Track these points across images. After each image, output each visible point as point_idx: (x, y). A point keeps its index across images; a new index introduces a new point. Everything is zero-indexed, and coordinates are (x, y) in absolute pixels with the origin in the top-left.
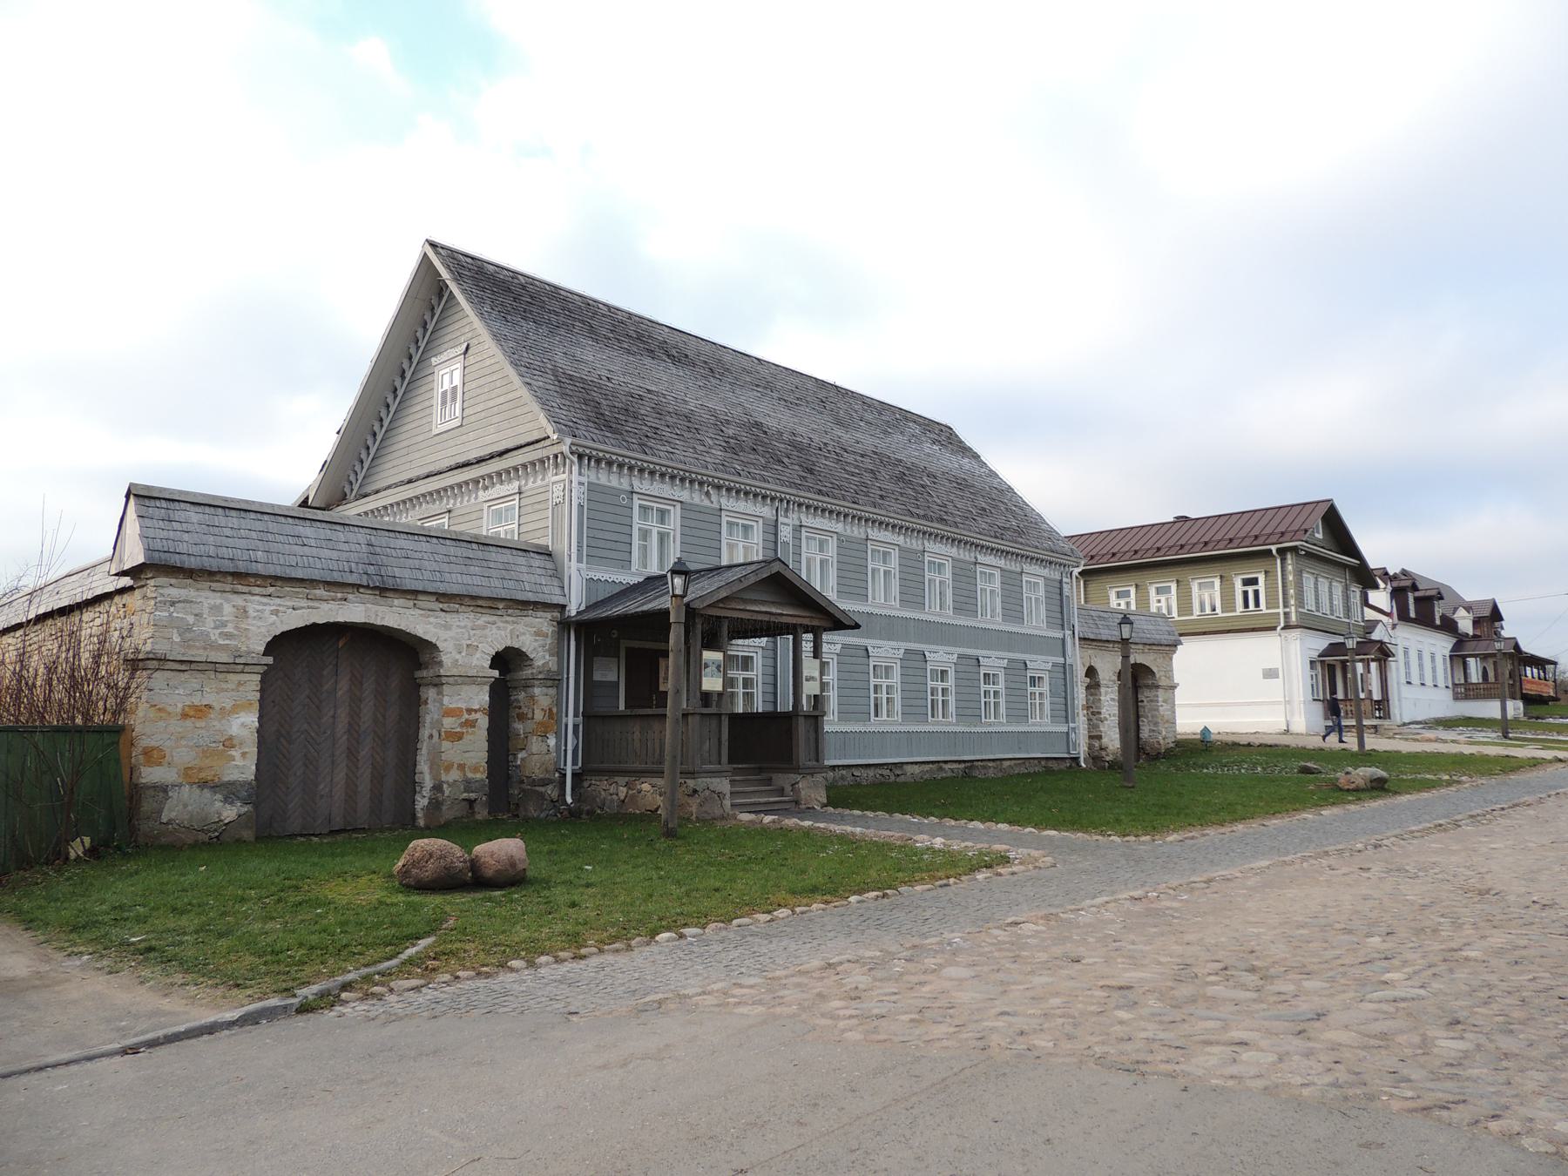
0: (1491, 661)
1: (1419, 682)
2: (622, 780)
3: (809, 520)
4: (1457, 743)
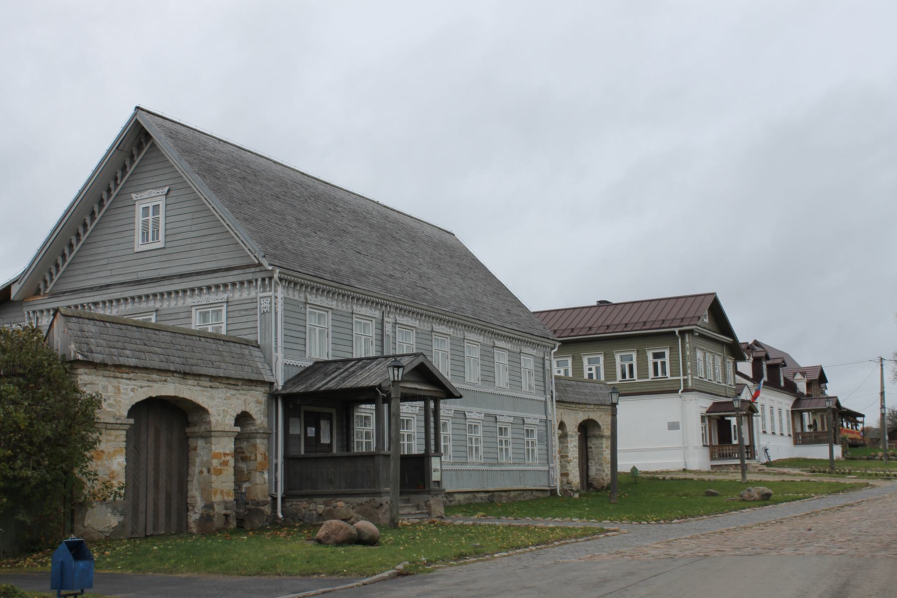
0: (819, 414)
1: (773, 430)
2: (320, 500)
3: (400, 320)
4: (797, 474)
